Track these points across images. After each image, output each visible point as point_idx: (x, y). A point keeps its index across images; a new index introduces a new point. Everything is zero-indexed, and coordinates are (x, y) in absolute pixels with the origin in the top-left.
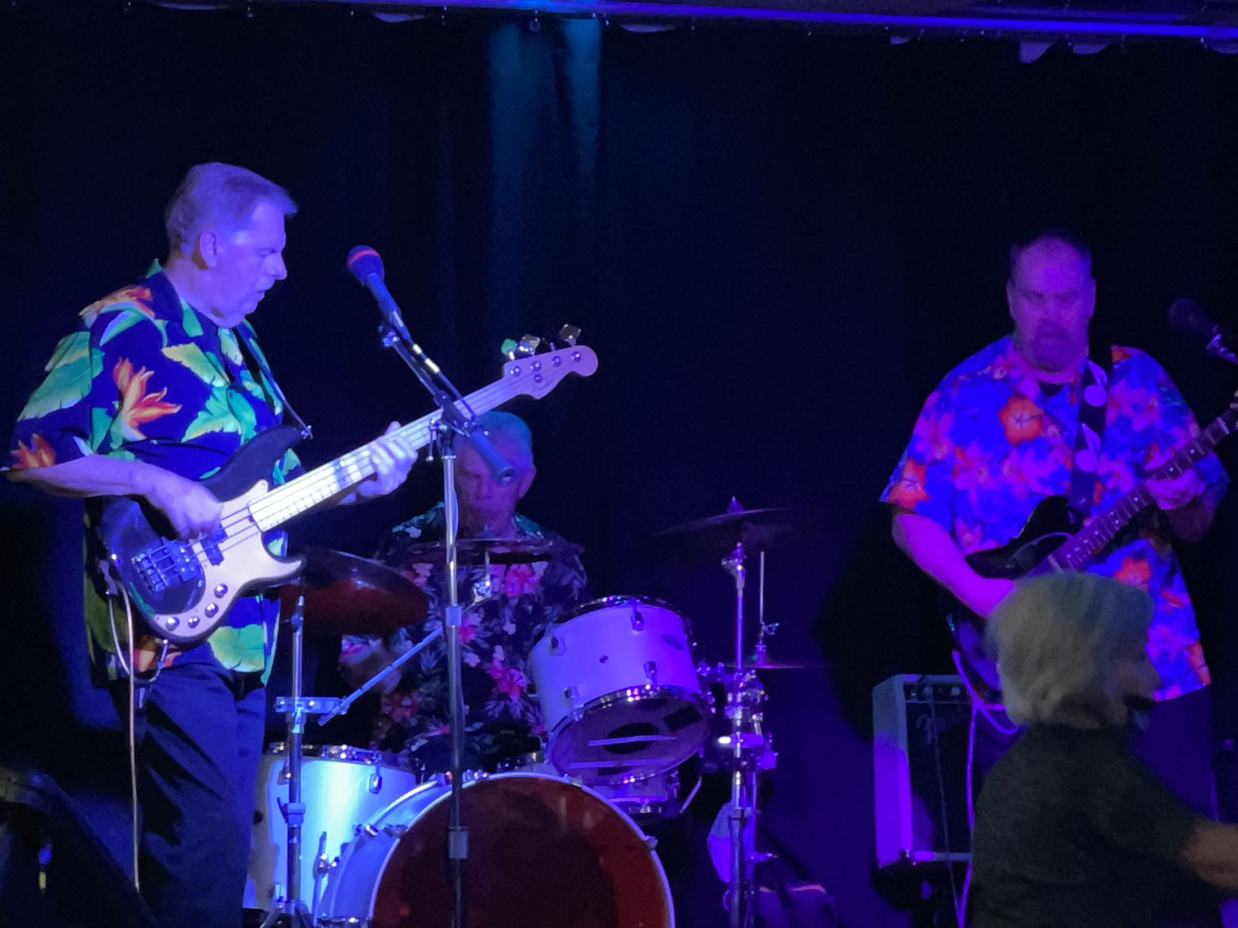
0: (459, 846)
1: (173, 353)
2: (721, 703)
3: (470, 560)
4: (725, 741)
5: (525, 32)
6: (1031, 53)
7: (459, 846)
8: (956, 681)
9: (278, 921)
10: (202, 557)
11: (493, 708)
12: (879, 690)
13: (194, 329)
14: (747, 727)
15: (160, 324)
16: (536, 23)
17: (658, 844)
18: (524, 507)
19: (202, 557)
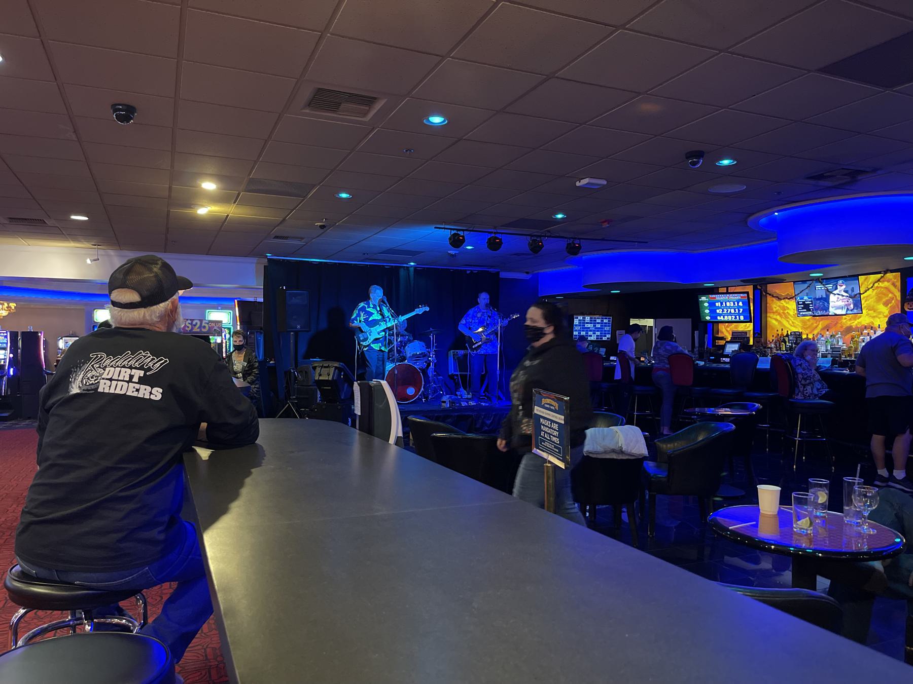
0: (396, 372)
1: (368, 309)
2: (429, 354)
3: (397, 336)
4: (430, 359)
5: (404, 269)
6: (468, 272)
7: (396, 372)
8: (852, 515)
9: (586, 514)
10: (369, 335)
11: (401, 355)
12: (449, 352)
13: (372, 306)
14: (433, 357)
15: (366, 306)
16: (405, 268)
17: (831, 583)
18: (405, 330)
19: (369, 335)
